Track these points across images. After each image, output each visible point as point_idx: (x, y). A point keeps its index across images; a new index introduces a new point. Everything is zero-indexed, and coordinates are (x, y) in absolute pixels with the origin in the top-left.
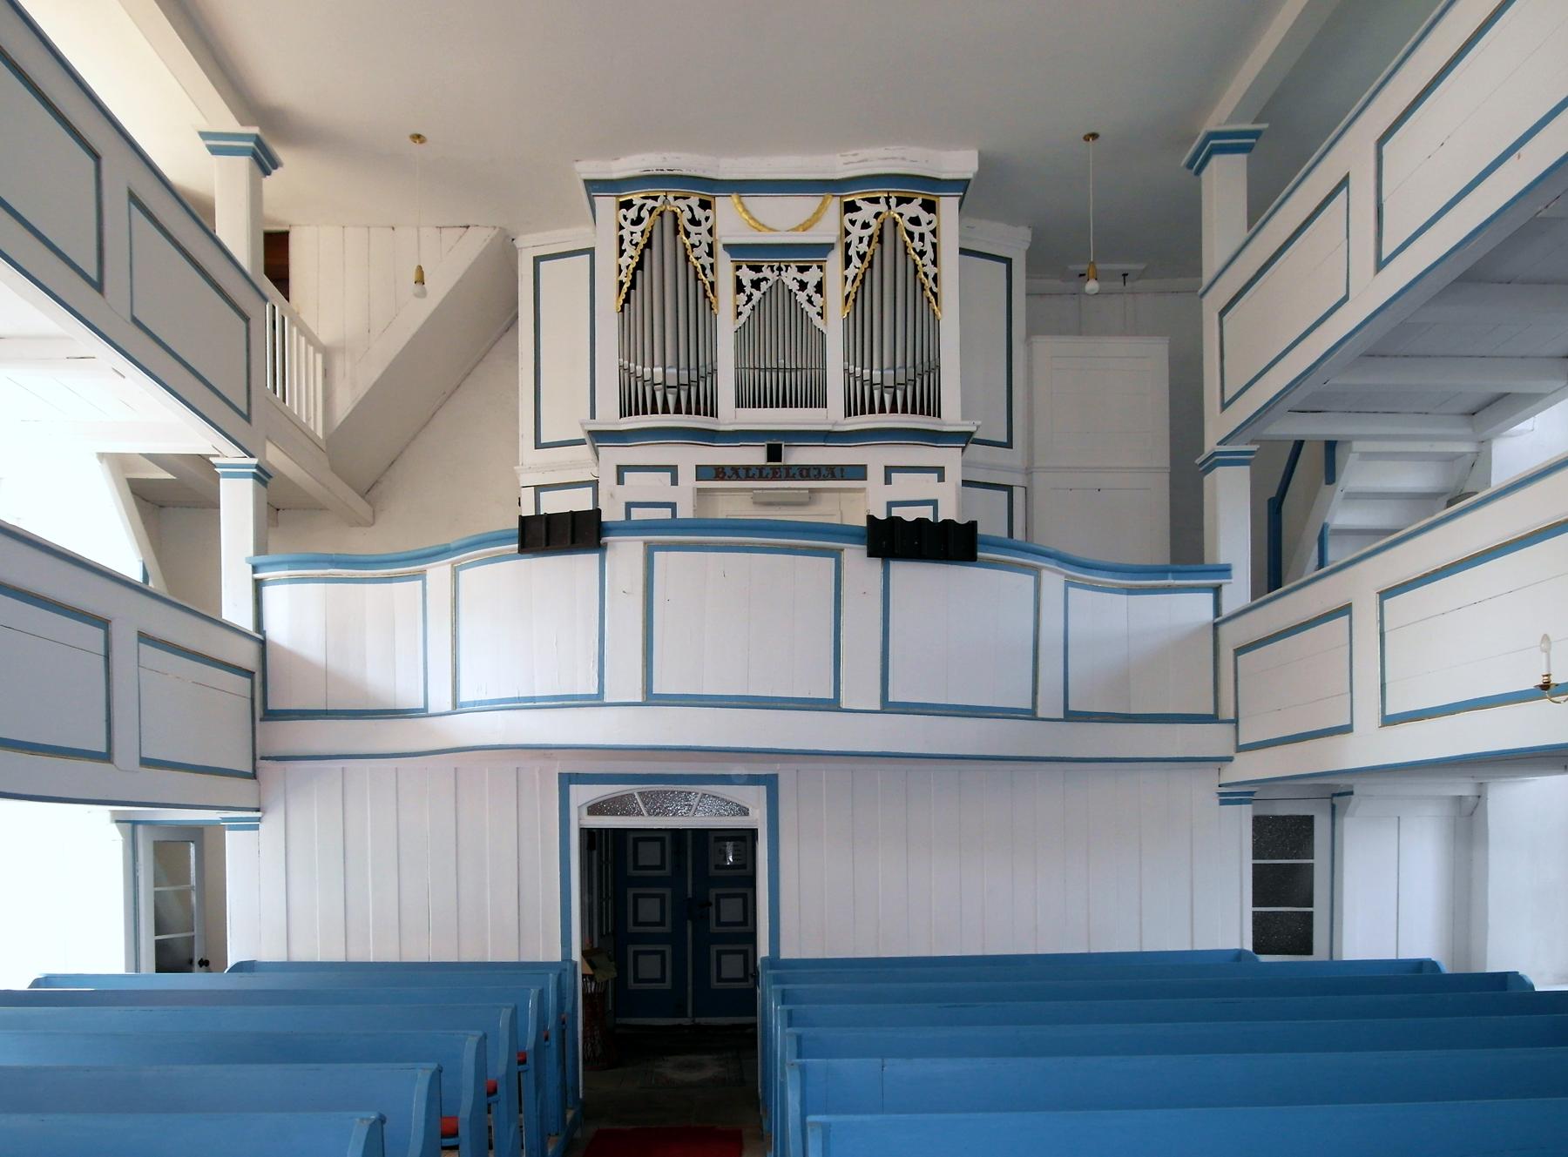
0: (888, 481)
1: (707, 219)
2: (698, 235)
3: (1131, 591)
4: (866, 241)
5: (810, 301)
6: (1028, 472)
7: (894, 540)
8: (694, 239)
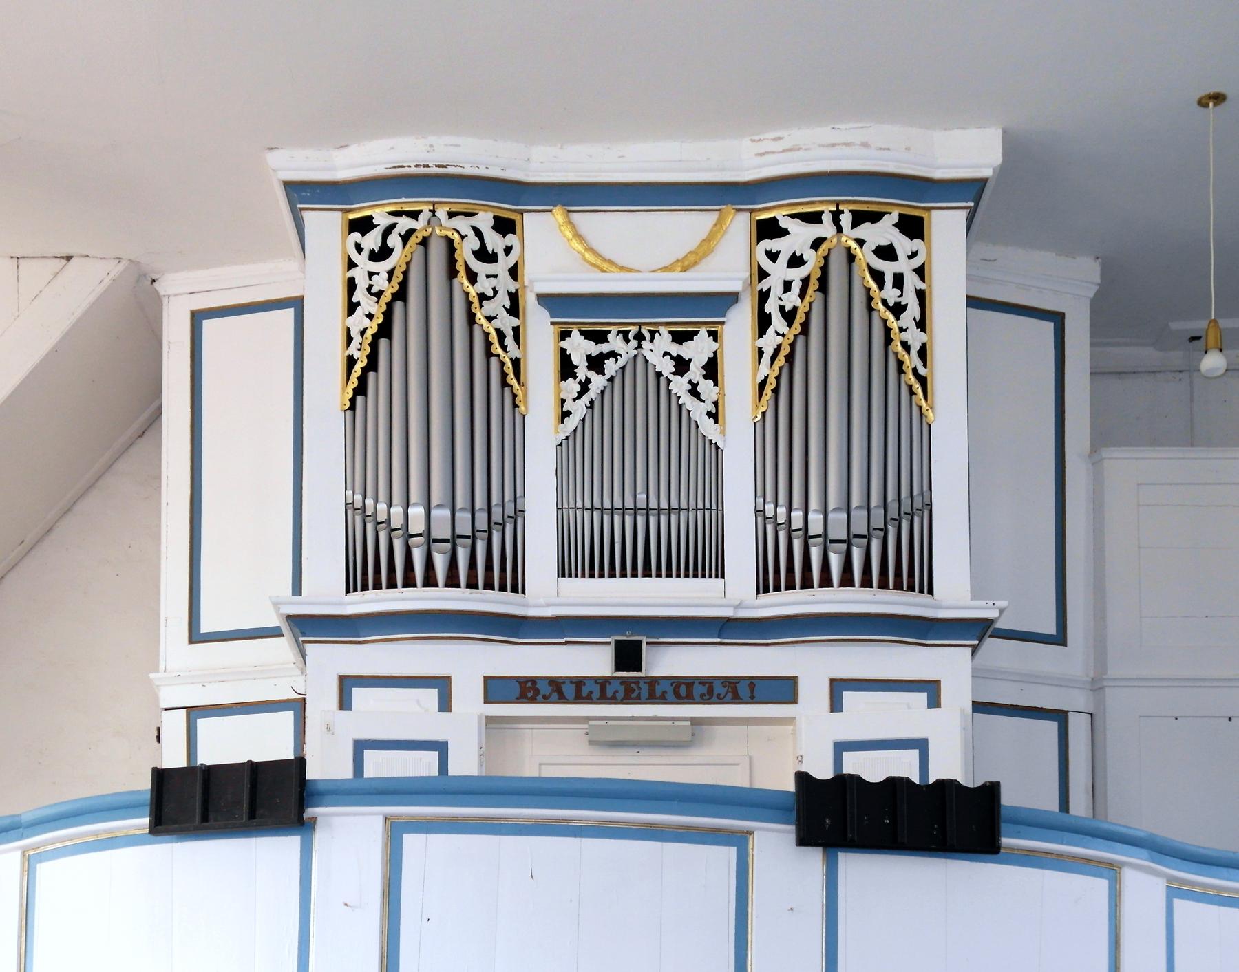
0: (836, 705)
1: (508, 250)
2: (492, 277)
4: (796, 287)
5: (694, 391)
6: (1097, 686)
7: (844, 816)
8: (484, 286)
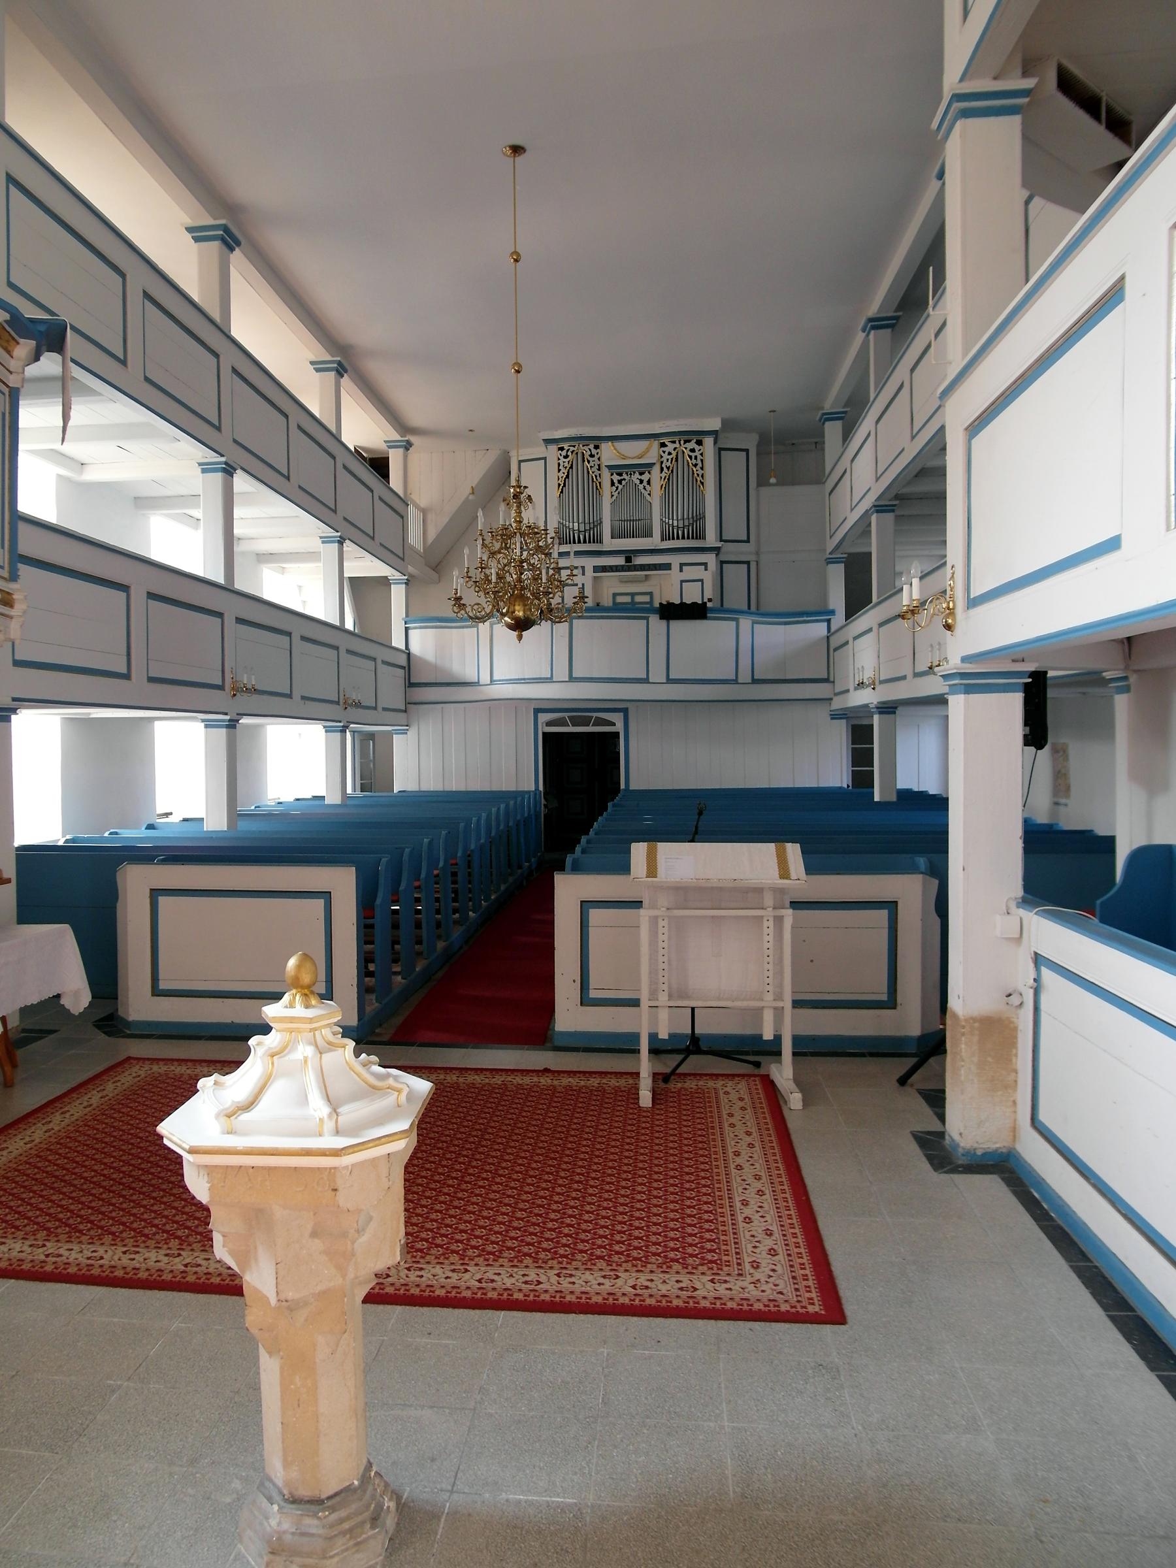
0: (681, 570)
3: (786, 623)
6: (757, 553)
7: (672, 612)
8: (592, 464)
